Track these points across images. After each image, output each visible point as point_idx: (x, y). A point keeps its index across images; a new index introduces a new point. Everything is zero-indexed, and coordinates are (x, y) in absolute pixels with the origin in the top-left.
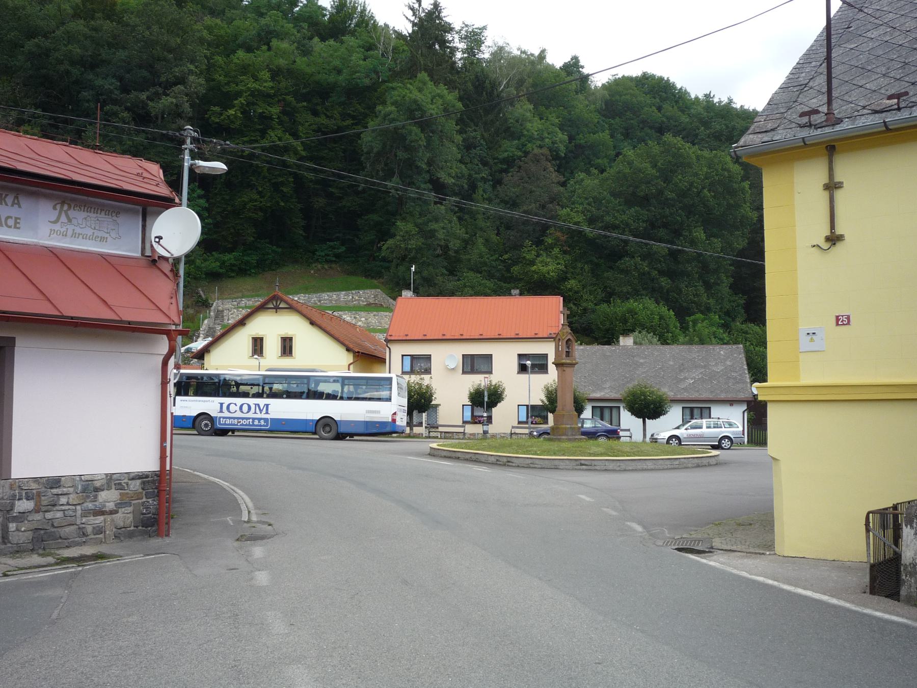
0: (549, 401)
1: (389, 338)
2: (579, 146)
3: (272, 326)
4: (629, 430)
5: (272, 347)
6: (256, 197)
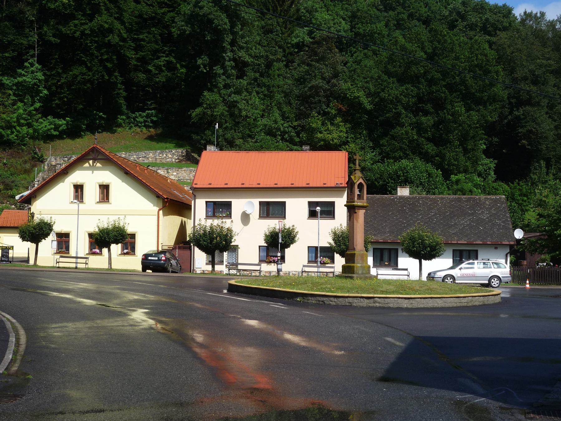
0: (335, 243)
1: (195, 186)
2: (357, 34)
3: (91, 177)
4: (406, 270)
5: (92, 193)
6: (84, 70)
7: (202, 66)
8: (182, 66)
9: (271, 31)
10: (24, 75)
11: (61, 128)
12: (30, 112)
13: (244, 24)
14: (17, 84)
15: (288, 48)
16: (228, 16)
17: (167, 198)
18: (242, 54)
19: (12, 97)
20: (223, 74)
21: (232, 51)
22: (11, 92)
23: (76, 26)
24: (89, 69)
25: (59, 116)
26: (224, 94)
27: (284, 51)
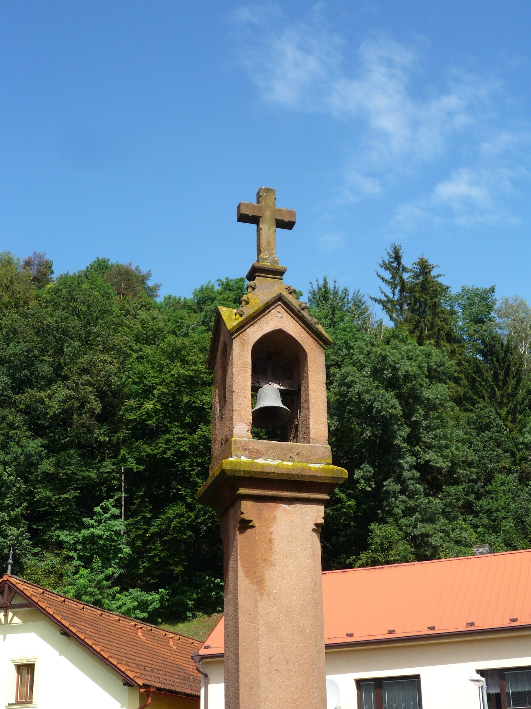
7: (362, 481)
8: (349, 497)
9: (488, 427)
10: (92, 526)
11: (151, 607)
12: (100, 582)
13: (431, 406)
14: (85, 541)
15: (520, 450)
16: (398, 396)
17: (144, 686)
18: (430, 455)
19: (77, 563)
20: (402, 492)
21: (415, 454)
22: (73, 554)
23: (167, 441)
24: (190, 507)
25: (148, 588)
26: (406, 526)
27: (513, 455)
